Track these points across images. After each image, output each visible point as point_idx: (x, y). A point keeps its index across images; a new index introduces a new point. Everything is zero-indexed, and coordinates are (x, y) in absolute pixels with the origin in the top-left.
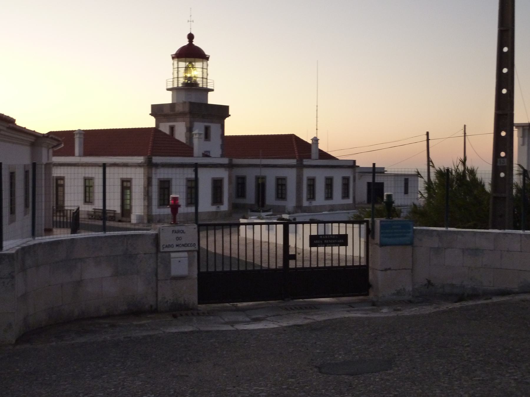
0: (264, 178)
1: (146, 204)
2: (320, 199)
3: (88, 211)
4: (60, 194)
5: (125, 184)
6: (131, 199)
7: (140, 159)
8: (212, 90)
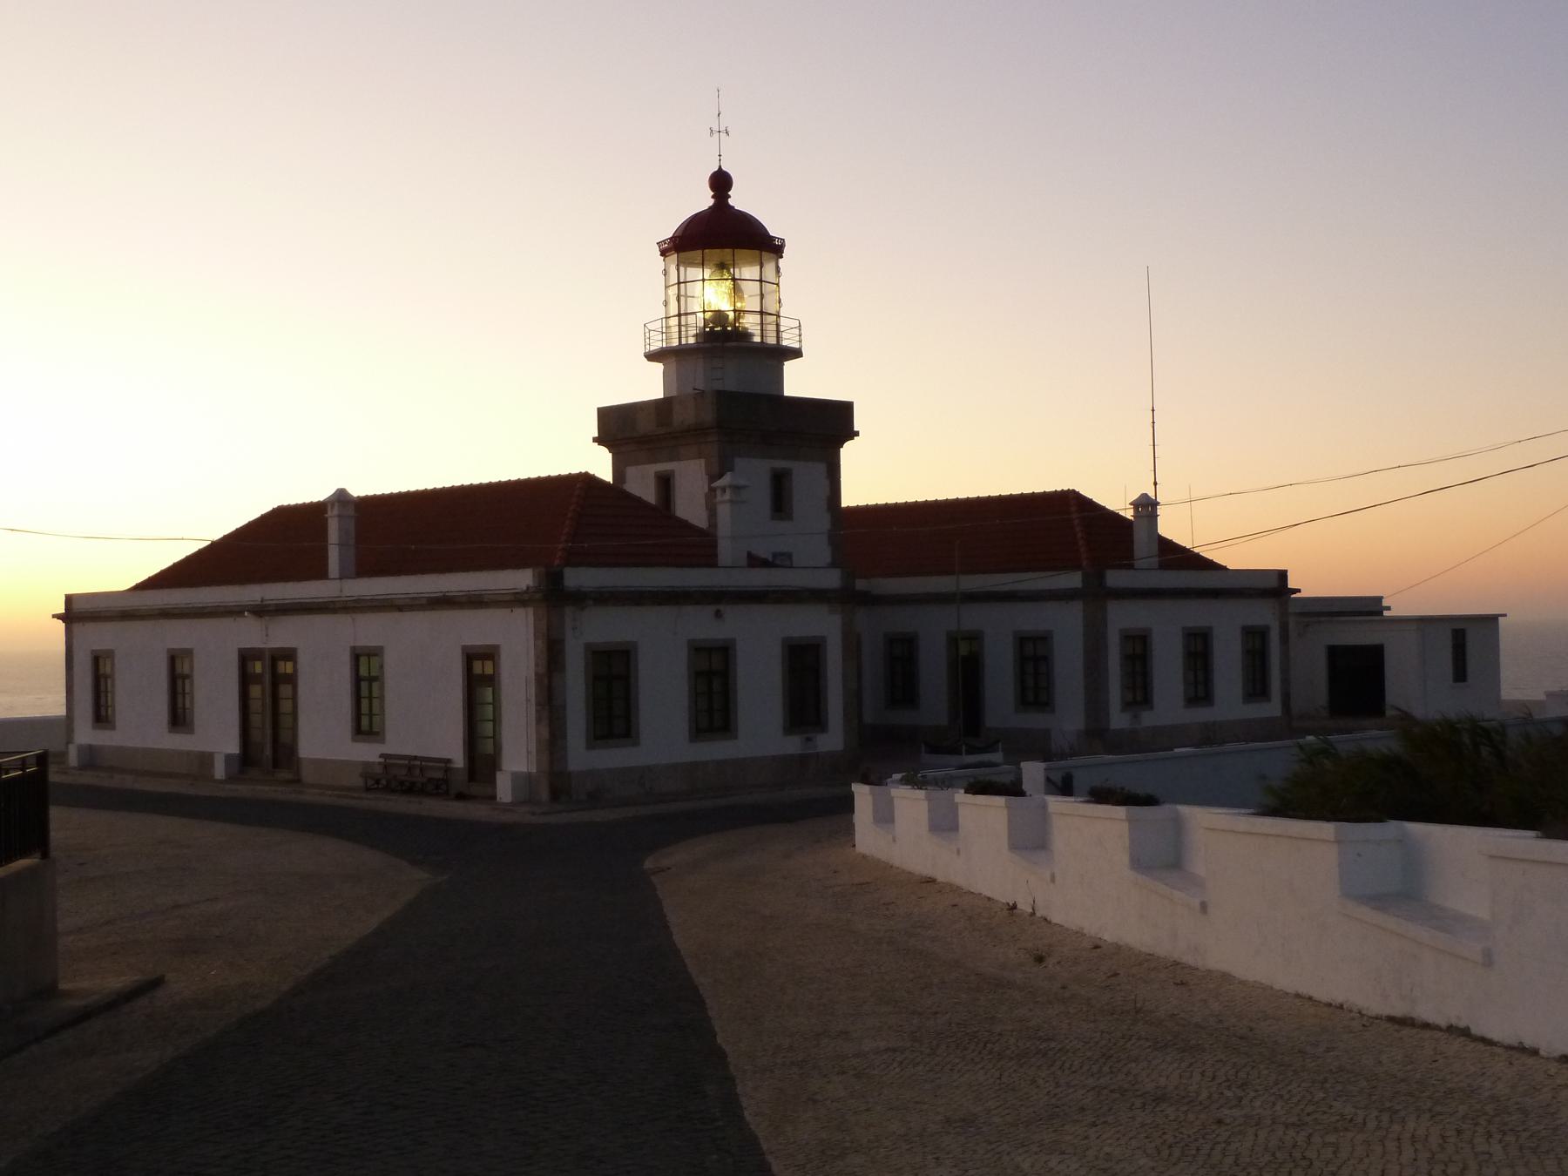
0: (975, 637)
1: (545, 733)
2: (1169, 702)
3: (366, 764)
4: (285, 706)
5: (477, 667)
6: (496, 720)
7: (522, 579)
8: (796, 353)
